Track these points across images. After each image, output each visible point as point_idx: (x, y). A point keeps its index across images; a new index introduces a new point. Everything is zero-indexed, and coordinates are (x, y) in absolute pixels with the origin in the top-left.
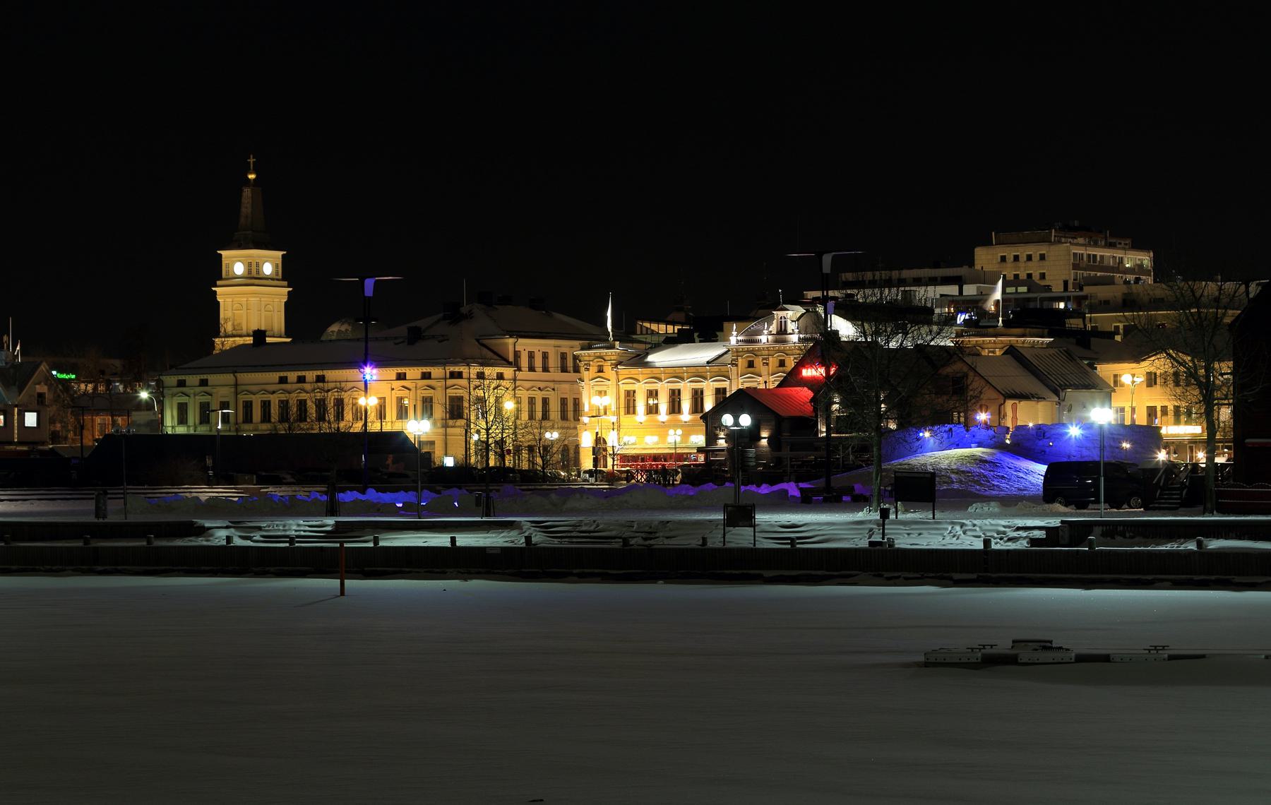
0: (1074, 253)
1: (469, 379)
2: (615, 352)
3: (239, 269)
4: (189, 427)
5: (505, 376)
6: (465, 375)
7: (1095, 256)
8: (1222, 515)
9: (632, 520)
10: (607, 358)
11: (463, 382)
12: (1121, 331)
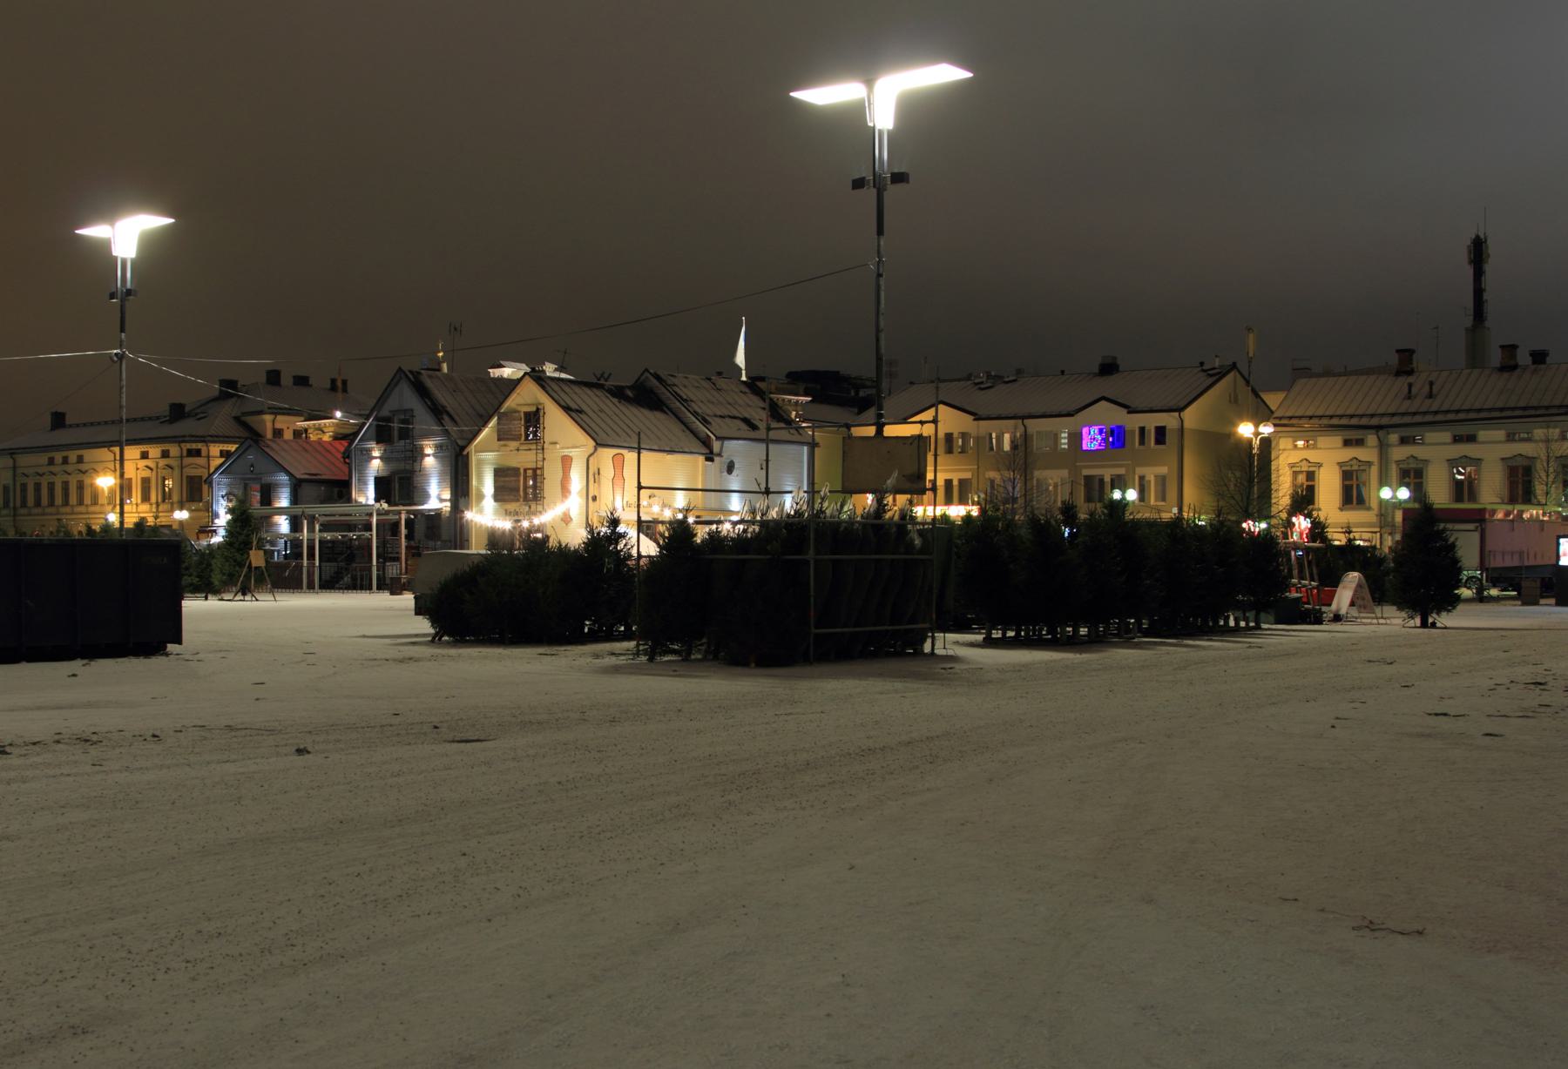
0: (1088, 479)
1: (208, 457)
2: (333, 423)
3: (1302, 523)
4: (151, 504)
5: (172, 454)
6: (204, 453)
7: (1297, 592)
8: (349, 523)
9: (1478, 457)
10: (325, 430)
11: (201, 461)
12: (119, 296)
